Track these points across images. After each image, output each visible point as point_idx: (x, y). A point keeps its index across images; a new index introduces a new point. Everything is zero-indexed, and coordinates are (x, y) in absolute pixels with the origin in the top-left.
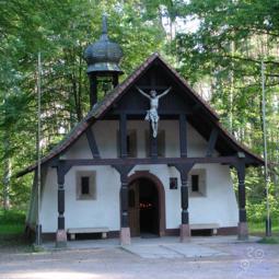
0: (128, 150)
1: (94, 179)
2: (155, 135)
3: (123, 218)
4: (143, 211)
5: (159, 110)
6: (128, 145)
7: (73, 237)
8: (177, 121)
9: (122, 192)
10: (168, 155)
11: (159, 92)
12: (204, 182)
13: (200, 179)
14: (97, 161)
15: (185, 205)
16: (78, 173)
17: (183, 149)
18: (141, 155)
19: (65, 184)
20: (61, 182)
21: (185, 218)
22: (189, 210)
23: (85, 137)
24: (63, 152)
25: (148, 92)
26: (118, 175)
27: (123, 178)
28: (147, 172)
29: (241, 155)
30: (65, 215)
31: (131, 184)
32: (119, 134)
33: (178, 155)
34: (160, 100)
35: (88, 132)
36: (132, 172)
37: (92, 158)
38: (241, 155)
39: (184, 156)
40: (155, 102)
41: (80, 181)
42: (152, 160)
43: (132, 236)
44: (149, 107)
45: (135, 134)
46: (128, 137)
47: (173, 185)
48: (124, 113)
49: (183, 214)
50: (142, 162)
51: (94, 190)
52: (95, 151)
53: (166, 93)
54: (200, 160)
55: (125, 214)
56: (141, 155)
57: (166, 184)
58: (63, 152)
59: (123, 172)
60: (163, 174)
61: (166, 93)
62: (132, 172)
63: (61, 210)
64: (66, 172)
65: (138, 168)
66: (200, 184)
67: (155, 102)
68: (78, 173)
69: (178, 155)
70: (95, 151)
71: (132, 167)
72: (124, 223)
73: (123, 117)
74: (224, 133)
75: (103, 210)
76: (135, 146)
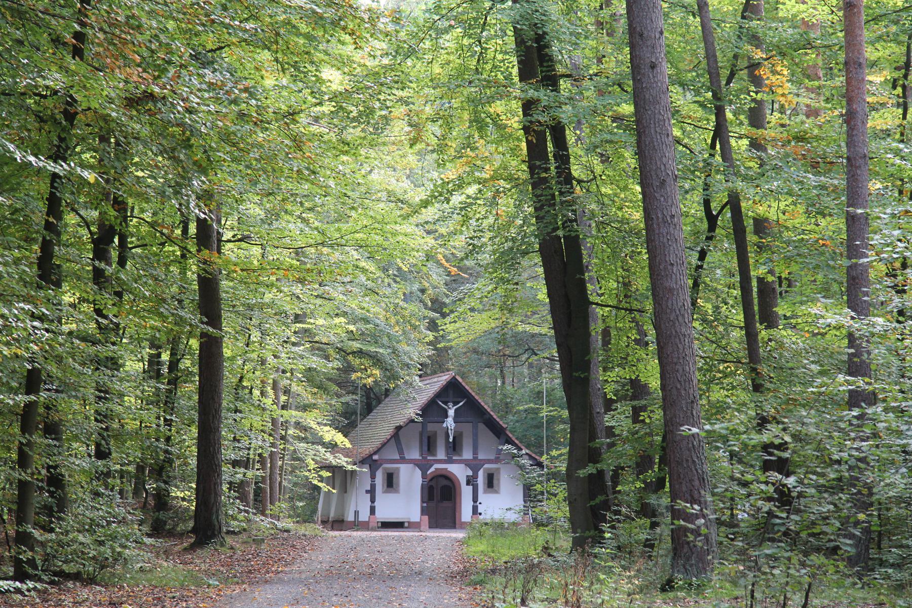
0: (429, 449)
1: (398, 477)
2: (451, 440)
3: (422, 508)
6: (429, 445)
11: (455, 403)
12: (499, 480)
14: (403, 460)
15: (475, 499)
17: (475, 452)
18: (441, 454)
21: (373, 511)
23: (393, 439)
24: (375, 453)
25: (446, 403)
26: (418, 473)
27: (424, 476)
30: (376, 504)
31: (431, 480)
32: (421, 434)
33: (471, 457)
34: (456, 410)
36: (432, 470)
39: (475, 458)
40: (451, 412)
42: (450, 461)
43: (430, 527)
44: (447, 416)
45: (435, 434)
46: (429, 438)
49: (473, 506)
51: (398, 485)
52: (401, 452)
53: (461, 404)
55: (425, 505)
56: (441, 454)
57: (463, 481)
58: (375, 453)
59: (424, 470)
60: (459, 471)
61: (461, 404)
62: (432, 470)
63: (373, 500)
64: (378, 469)
65: (437, 466)
66: (495, 482)
67: (451, 412)
70: (401, 452)
71: (431, 466)
76: (435, 447)
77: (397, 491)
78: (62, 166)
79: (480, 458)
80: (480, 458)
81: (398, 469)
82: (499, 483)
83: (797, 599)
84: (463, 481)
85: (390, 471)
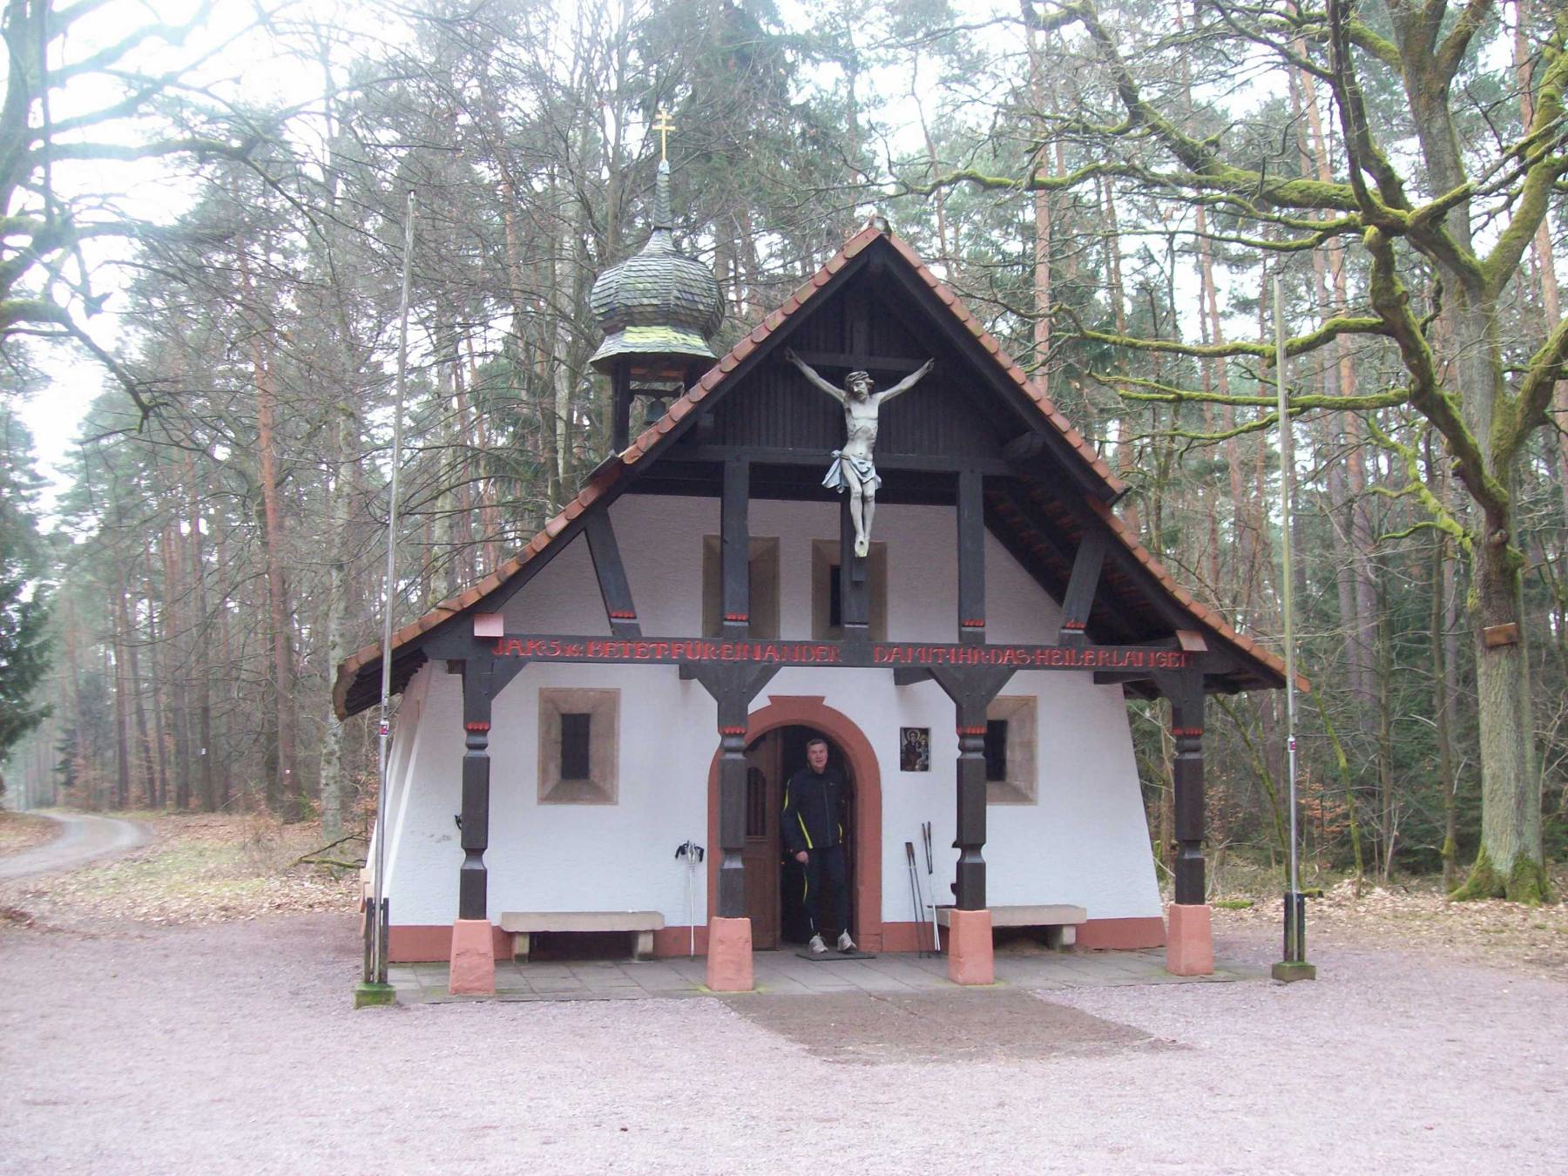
1: (611, 733)
2: (861, 551)
4: (1173, 847)
5: (881, 446)
7: (522, 946)
8: (949, 512)
9: (721, 773)
10: (898, 631)
11: (882, 380)
12: (1029, 746)
13: (1013, 738)
16: (549, 699)
19: (491, 737)
20: (477, 722)
21: (970, 887)
22: (987, 853)
25: (838, 377)
27: (731, 714)
28: (817, 701)
29: (1193, 643)
30: (490, 859)
33: (947, 634)
34: (884, 409)
35: (592, 523)
37: (610, 634)
38: (1193, 643)
39: (971, 641)
40: (864, 417)
41: (595, 771)
43: (760, 946)
44: (841, 436)
47: (914, 753)
48: (738, 461)
50: (799, 655)
52: (616, 596)
53: (908, 382)
54: (1033, 658)
56: (797, 623)
57: (887, 752)
58: (487, 605)
61: (908, 382)
63: (475, 845)
64: (494, 688)
67: (864, 417)
68: (549, 699)
69: (947, 634)
70: (616, 596)
71: (768, 673)
72: (726, 899)
73: (737, 480)
74: (1126, 552)
75: (1174, 842)
77: (602, 795)
78: (163, 772)
79: (990, 640)
80: (990, 640)
81: (610, 699)
82: (1031, 759)
83: (1565, 936)
84: (887, 752)
85: (580, 708)
